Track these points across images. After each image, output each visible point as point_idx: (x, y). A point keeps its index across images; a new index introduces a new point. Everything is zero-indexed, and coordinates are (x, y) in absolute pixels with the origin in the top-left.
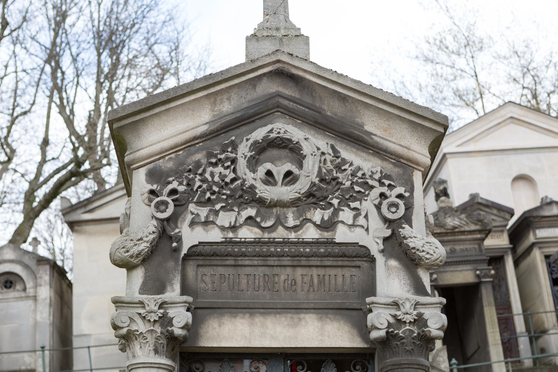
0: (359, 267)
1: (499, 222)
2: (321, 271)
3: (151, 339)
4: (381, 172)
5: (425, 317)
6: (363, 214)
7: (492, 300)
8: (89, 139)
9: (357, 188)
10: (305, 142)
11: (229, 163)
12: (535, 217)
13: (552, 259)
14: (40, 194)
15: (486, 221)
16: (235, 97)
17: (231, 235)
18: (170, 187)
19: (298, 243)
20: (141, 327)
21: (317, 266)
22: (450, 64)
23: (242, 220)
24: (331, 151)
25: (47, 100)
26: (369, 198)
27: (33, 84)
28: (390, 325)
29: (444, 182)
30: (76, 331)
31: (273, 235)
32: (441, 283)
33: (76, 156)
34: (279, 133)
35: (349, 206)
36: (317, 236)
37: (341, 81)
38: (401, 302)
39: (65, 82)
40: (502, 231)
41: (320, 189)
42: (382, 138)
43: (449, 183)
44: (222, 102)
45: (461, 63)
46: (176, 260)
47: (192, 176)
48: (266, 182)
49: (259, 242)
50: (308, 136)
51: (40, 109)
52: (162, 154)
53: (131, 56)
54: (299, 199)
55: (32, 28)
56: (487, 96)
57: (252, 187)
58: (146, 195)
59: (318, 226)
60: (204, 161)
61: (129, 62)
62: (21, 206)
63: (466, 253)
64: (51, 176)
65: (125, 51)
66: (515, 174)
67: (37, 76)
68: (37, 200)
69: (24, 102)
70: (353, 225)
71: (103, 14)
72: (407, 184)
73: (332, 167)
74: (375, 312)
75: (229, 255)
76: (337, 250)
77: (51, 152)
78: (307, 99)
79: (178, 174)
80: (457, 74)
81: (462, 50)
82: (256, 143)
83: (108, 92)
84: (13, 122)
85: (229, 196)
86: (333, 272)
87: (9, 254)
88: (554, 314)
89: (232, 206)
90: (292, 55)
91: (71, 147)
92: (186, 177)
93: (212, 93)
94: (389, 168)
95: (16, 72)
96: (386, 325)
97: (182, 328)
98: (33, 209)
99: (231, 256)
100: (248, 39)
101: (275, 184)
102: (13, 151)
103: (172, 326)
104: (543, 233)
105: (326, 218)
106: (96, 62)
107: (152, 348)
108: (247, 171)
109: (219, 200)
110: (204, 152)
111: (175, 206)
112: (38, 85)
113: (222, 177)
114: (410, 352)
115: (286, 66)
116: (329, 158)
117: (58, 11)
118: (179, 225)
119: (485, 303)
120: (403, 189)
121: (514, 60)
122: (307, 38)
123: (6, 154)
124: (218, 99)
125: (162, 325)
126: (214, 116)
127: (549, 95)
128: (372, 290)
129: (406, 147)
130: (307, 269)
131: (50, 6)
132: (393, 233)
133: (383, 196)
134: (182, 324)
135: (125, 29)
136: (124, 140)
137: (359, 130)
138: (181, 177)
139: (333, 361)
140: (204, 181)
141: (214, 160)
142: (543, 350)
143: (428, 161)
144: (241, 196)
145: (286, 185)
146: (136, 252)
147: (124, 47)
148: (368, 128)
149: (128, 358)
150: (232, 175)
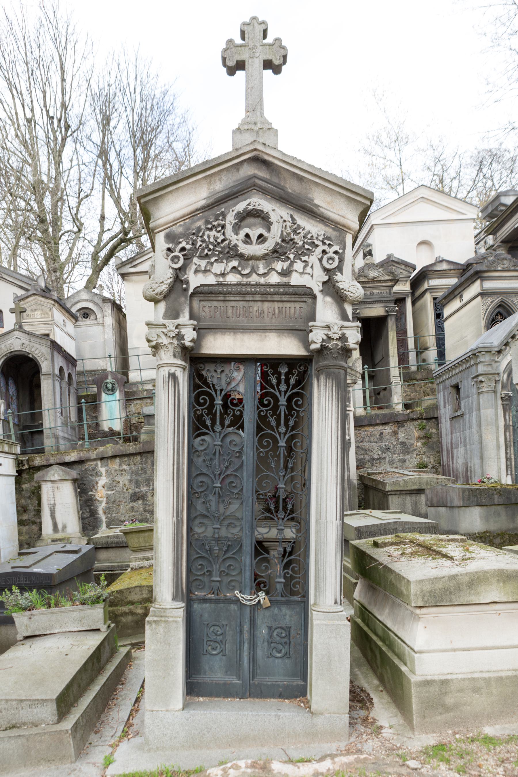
0: (306, 302)
1: (405, 274)
2: (280, 305)
3: (171, 348)
4: (324, 235)
5: (347, 335)
6: (310, 265)
7: (394, 327)
8: (132, 215)
9: (307, 247)
10: (272, 212)
11: (220, 228)
12: (430, 271)
13: (438, 300)
14: (103, 254)
15: (396, 273)
16: (224, 178)
17: (221, 279)
18: (181, 246)
19: (266, 285)
20: (164, 340)
21: (278, 301)
22: (383, 156)
23: (228, 269)
24: (290, 219)
25: (101, 186)
26: (314, 254)
27: (92, 174)
28: (323, 341)
29: (370, 245)
30: (130, 345)
31: (249, 280)
32: (362, 315)
33: (124, 228)
34: (254, 206)
35: (301, 259)
36: (278, 281)
37: (299, 165)
38: (331, 325)
39: (113, 173)
40: (406, 281)
41: (282, 247)
42: (326, 209)
43: (373, 246)
44: (215, 183)
45: (391, 154)
46: (186, 297)
47: (195, 238)
48: (245, 242)
49: (240, 284)
50: (274, 208)
51: (97, 194)
52: (175, 222)
53: (157, 152)
54: (267, 254)
55: (86, 130)
56: (407, 182)
57: (236, 246)
58: (165, 252)
59: (279, 274)
60: (203, 227)
61: (156, 156)
62: (90, 264)
63: (380, 296)
64: (108, 243)
65: (153, 147)
66: (419, 241)
67: (93, 168)
68: (100, 259)
69: (86, 187)
70: (303, 273)
71: (136, 118)
72: (341, 244)
73: (290, 231)
74: (314, 331)
75: (220, 293)
76: (291, 290)
77: (107, 225)
78: (275, 180)
79: (185, 236)
80: (387, 164)
81: (393, 145)
82: (239, 213)
83: (142, 180)
84: (80, 204)
85: (220, 252)
86: (288, 305)
87: (85, 296)
88: (434, 337)
89: (222, 259)
90: (265, 144)
91: (120, 221)
92: (191, 239)
93: (209, 175)
94: (330, 232)
95: (79, 165)
96: (321, 340)
97: (191, 341)
98: (98, 265)
99: (221, 294)
100: (234, 132)
101: (251, 243)
102: (82, 224)
103: (184, 340)
104: (433, 282)
105: (285, 268)
106: (133, 156)
107: (172, 354)
108: (232, 234)
109: (213, 255)
110: (203, 221)
111: (184, 259)
112: (94, 175)
113: (216, 238)
114: (336, 358)
115: (261, 154)
116: (288, 224)
117: (103, 116)
118: (187, 272)
119: (390, 329)
120: (338, 247)
121: (430, 152)
122: (277, 131)
123: (77, 226)
124: (213, 179)
125: (178, 340)
126: (210, 193)
127: (452, 181)
128: (313, 318)
129: (343, 217)
130: (271, 303)
131: (98, 111)
132: (329, 279)
133: (324, 252)
134: (190, 339)
135: (152, 131)
136: (148, 211)
137: (310, 203)
138: (188, 238)
139: (286, 364)
140: (203, 241)
141: (210, 226)
142: (424, 361)
143: (356, 226)
144: (228, 252)
145: (259, 244)
146: (160, 291)
147: (152, 144)
148: (317, 202)
149: (157, 360)
150: (222, 237)
